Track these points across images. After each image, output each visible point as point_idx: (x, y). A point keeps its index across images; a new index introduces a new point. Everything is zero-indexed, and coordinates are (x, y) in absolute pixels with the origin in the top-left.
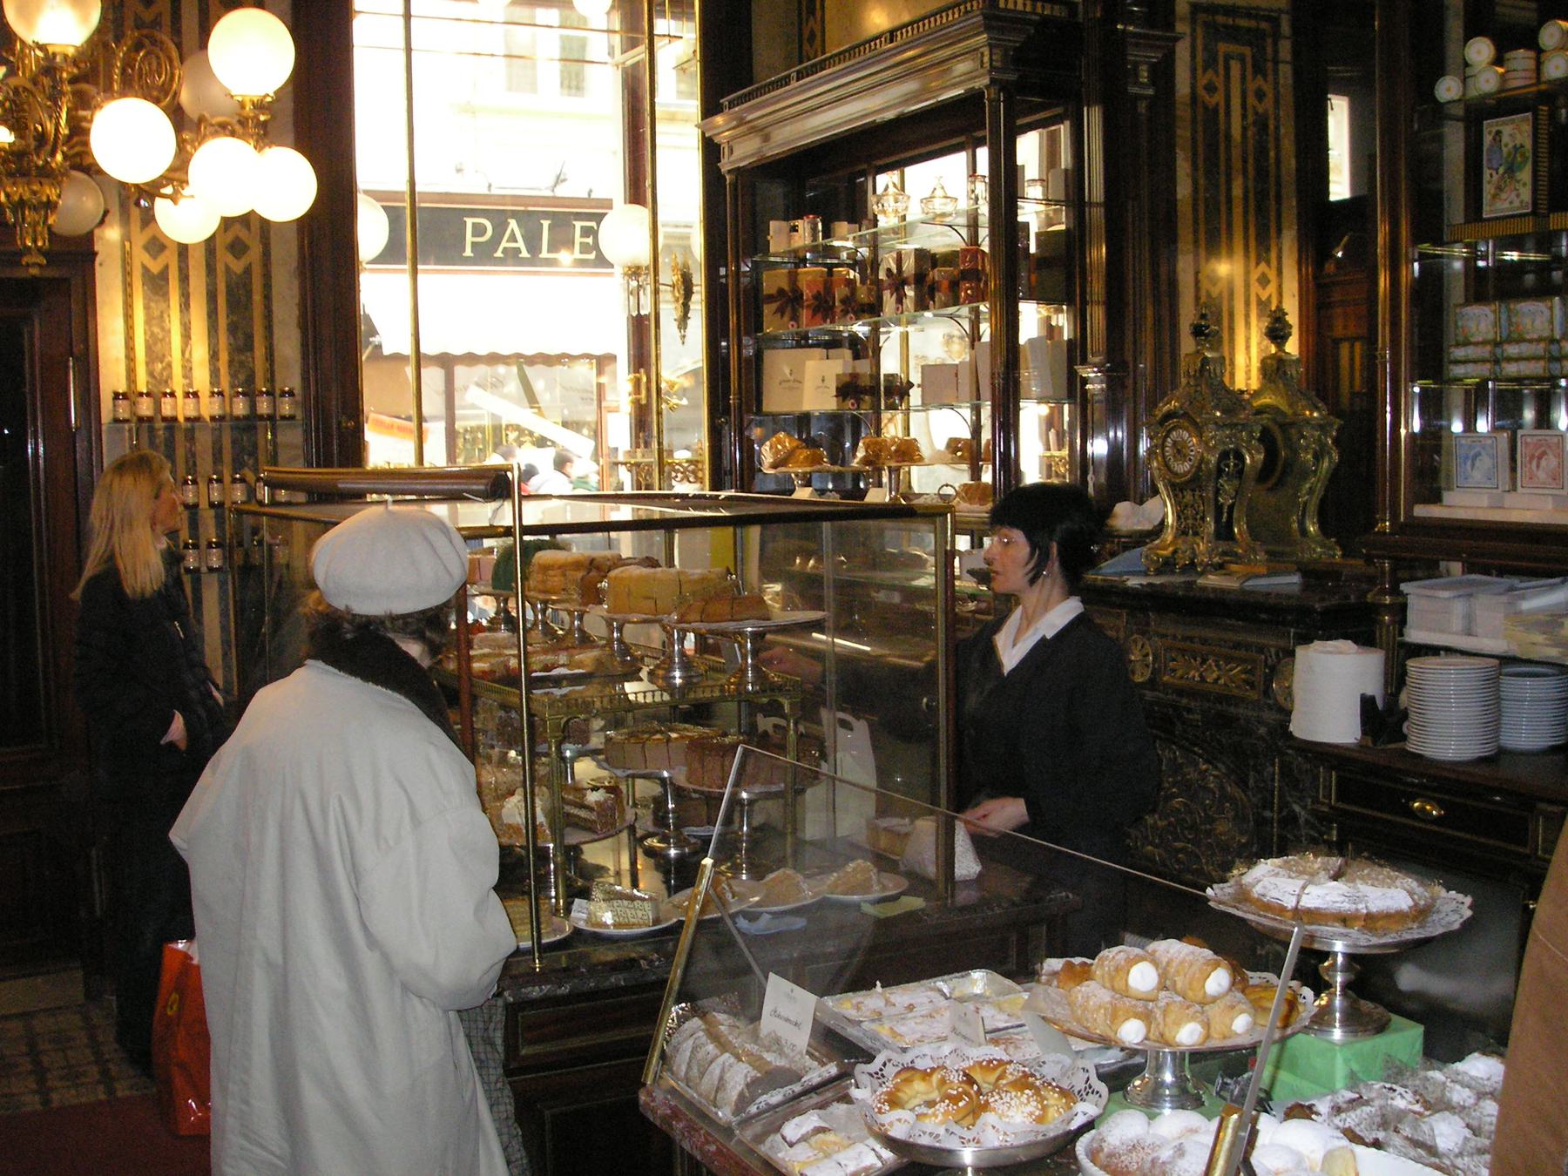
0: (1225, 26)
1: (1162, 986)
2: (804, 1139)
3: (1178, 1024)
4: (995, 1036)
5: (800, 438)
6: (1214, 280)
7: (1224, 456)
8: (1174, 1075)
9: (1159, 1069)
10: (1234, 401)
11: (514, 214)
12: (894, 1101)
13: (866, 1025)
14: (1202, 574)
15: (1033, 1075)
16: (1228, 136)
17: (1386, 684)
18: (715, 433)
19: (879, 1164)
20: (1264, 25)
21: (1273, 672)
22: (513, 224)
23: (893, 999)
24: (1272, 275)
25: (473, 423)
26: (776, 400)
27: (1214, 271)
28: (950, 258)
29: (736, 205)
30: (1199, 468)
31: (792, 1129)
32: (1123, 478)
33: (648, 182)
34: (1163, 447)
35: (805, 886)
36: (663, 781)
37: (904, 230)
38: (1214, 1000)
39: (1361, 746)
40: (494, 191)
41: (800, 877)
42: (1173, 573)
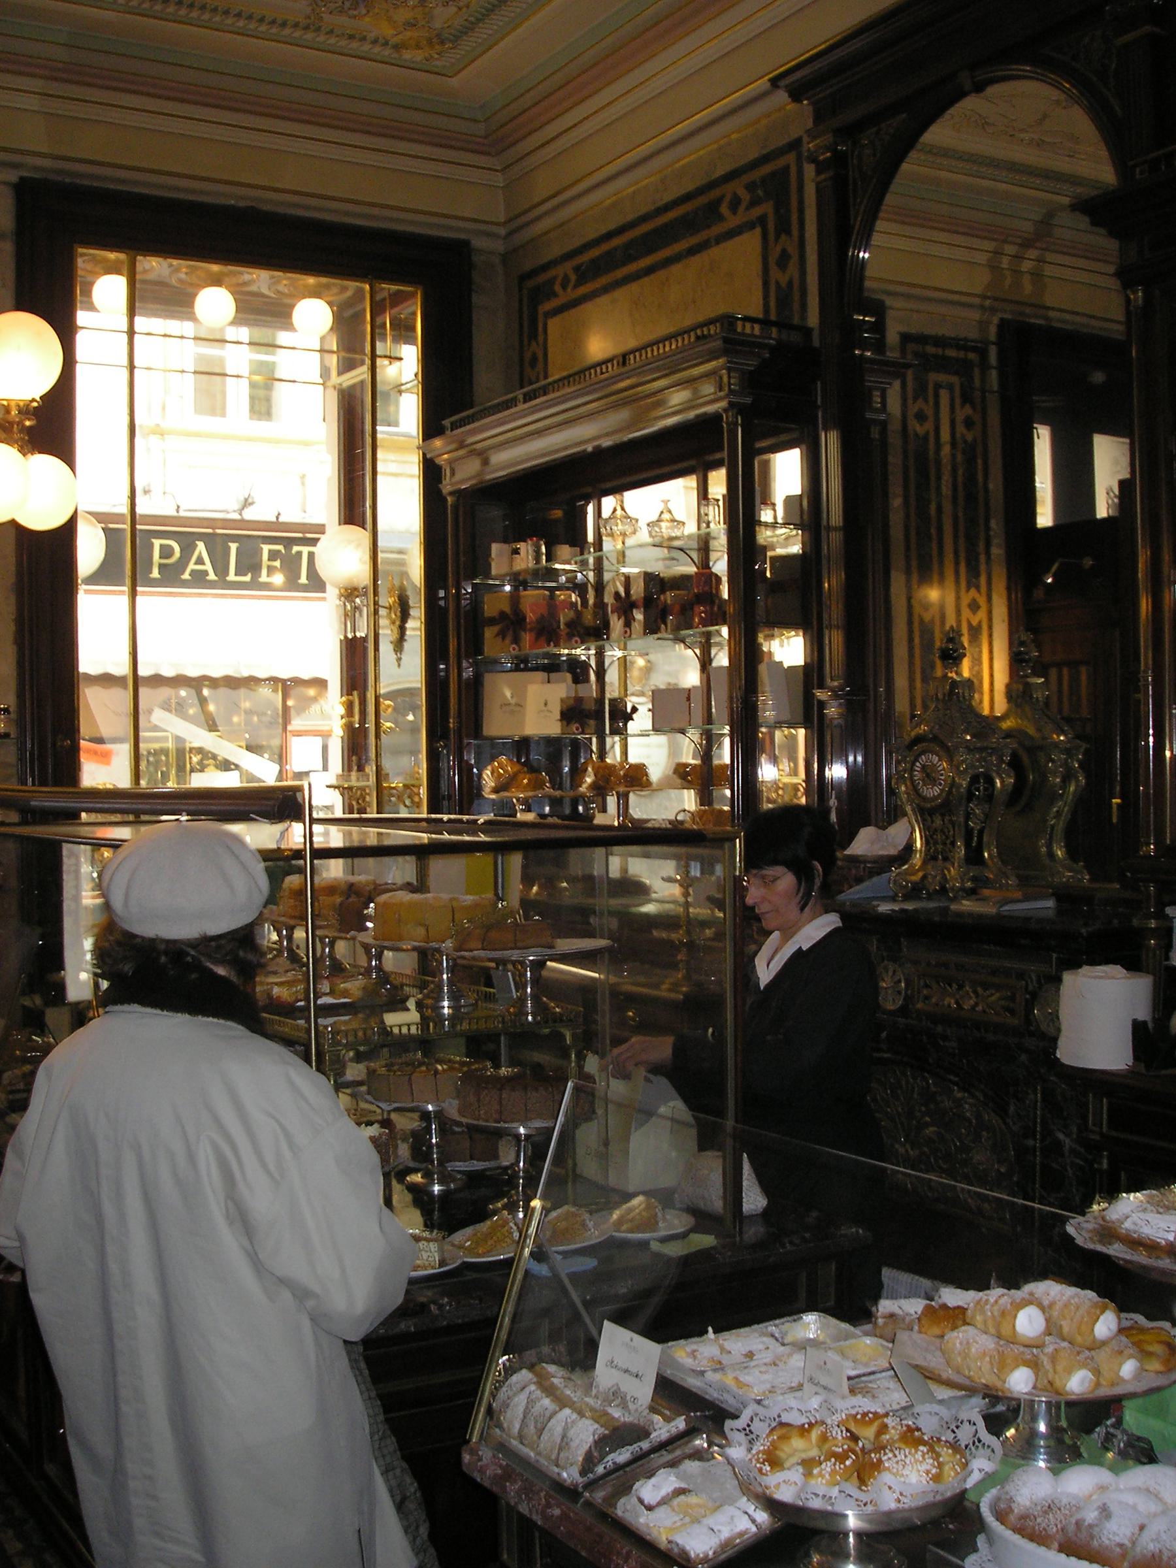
0: (935, 356)
1: (1048, 1332)
2: (663, 1502)
3: (1069, 1372)
4: (856, 1385)
5: (519, 761)
6: (926, 606)
7: (975, 779)
8: (1048, 1425)
9: (1034, 1419)
10: (985, 726)
11: (201, 537)
12: (774, 1461)
13: (710, 1376)
14: (954, 899)
15: (918, 1429)
16: (938, 462)
17: (1155, 1007)
18: (433, 757)
19: (754, 1529)
20: (972, 356)
21: (1034, 997)
22: (201, 546)
23: (728, 1345)
24: (982, 601)
25: (157, 746)
26: (497, 725)
27: (926, 597)
28: (681, 581)
29: (455, 526)
30: (950, 793)
31: (651, 1489)
32: (862, 803)
33: (368, 503)
34: (912, 770)
35: (590, 1224)
36: (425, 1116)
37: (622, 557)
38: (1104, 1343)
39: (1132, 1072)
40: (182, 514)
41: (586, 1216)
42: (920, 899)
